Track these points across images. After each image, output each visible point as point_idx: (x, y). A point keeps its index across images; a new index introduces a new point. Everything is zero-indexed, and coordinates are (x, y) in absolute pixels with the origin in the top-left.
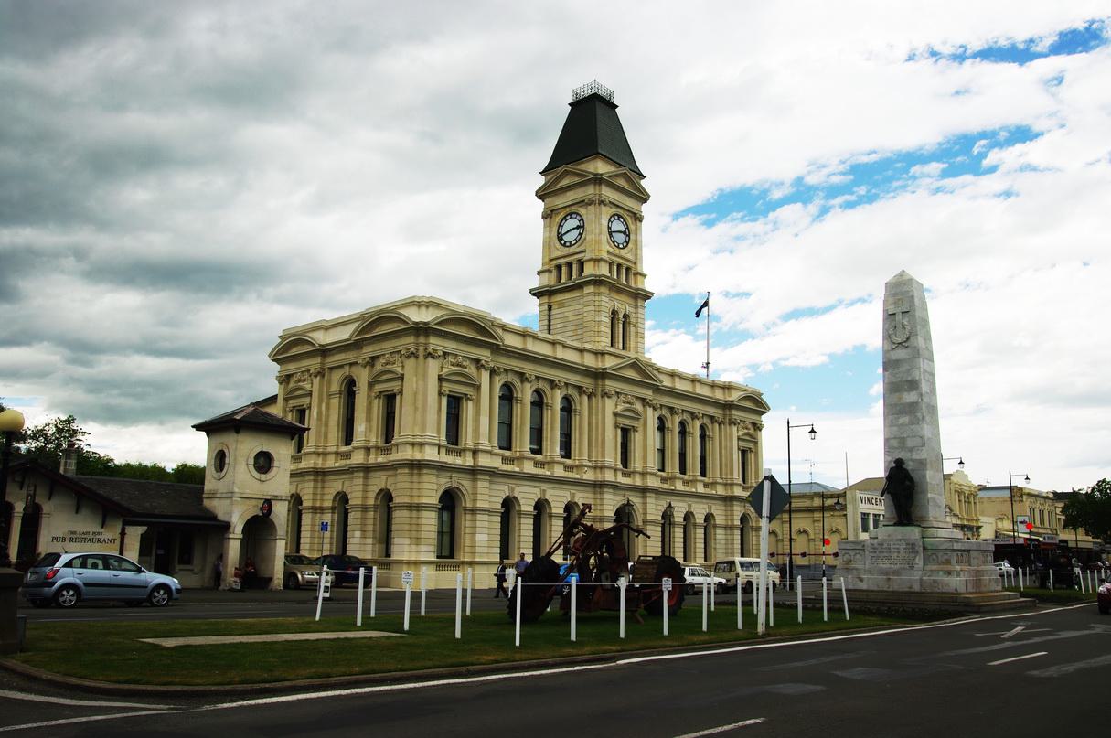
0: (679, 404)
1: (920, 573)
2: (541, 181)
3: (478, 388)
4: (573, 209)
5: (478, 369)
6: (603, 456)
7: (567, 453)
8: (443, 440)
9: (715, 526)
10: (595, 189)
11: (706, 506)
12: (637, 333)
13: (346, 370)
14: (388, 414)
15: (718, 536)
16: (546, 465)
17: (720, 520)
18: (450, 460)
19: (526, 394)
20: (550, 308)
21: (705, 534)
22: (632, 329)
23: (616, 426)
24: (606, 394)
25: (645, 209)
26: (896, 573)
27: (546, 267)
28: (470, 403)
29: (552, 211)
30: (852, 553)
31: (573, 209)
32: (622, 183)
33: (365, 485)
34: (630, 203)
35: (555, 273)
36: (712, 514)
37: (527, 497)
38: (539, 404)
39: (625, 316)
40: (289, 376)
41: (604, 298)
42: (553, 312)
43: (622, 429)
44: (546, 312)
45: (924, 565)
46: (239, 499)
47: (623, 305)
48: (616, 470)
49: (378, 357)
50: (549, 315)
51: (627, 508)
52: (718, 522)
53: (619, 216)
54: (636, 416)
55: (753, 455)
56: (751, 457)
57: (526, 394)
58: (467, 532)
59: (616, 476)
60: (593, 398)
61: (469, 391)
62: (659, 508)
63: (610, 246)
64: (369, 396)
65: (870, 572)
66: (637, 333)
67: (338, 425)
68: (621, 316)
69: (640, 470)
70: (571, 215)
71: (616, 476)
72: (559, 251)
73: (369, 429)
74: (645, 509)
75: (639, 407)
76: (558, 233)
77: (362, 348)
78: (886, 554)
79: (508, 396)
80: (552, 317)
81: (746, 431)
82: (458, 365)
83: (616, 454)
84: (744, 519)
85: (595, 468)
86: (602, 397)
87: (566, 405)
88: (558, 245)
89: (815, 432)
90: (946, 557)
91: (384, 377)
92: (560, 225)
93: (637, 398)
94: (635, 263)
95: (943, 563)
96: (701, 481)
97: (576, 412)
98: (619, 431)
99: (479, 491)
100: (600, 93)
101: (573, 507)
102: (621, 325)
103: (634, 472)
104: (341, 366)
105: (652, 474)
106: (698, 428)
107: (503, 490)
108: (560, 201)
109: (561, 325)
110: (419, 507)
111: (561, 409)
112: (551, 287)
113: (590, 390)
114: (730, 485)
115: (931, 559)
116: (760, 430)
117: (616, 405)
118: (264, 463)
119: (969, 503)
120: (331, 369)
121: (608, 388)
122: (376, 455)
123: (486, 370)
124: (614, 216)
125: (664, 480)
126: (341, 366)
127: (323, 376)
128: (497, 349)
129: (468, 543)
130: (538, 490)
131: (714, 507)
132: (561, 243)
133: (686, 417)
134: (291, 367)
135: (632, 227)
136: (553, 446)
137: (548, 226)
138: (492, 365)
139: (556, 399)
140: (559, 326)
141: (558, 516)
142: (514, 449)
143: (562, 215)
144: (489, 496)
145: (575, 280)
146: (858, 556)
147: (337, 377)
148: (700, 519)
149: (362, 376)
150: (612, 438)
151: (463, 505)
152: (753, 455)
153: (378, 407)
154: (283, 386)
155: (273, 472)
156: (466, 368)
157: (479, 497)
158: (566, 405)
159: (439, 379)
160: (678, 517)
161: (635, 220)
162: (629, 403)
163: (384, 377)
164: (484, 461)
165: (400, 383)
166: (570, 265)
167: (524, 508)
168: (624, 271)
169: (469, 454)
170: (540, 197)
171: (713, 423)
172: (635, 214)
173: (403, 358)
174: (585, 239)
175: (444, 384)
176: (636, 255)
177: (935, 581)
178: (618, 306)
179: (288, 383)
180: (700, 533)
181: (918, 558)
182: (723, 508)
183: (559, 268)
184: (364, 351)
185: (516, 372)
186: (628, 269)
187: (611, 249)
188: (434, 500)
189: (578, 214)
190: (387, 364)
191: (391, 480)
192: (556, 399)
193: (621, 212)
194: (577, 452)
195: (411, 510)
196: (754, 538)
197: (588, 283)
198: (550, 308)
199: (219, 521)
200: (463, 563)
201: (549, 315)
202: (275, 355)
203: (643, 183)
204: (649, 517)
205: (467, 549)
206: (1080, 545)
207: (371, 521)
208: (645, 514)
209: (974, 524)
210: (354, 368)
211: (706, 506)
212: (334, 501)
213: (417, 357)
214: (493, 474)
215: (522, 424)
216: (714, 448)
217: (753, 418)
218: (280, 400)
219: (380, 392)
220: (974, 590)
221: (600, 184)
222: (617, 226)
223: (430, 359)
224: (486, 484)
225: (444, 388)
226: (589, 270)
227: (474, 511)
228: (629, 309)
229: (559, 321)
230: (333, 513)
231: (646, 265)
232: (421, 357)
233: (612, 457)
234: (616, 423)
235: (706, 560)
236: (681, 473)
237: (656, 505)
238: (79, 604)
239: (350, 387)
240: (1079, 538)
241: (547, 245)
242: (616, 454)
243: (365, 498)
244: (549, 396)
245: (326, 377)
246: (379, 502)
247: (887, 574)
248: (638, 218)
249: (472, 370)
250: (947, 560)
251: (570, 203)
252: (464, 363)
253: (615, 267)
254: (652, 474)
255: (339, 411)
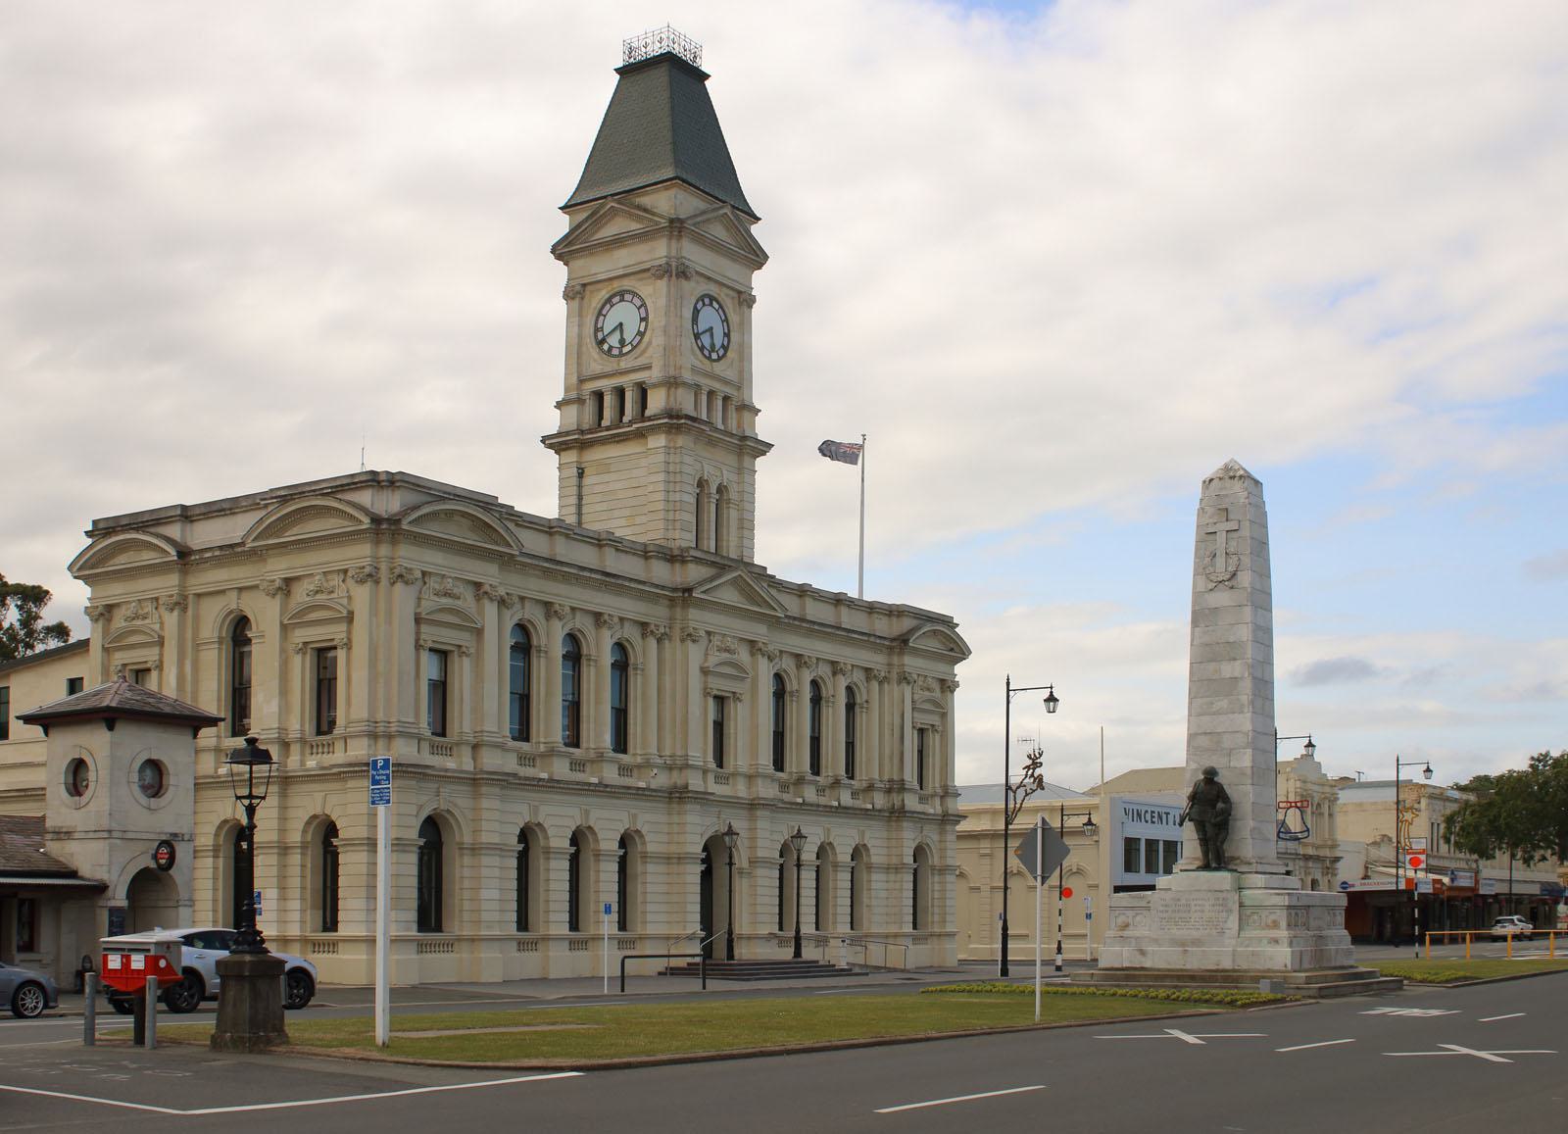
0: (566, 595)
1: (1234, 942)
2: (562, 225)
3: (479, 632)
4: (626, 284)
5: (478, 598)
6: (685, 747)
7: (621, 743)
8: (424, 727)
9: (869, 867)
10: (669, 246)
11: (576, 812)
12: (741, 520)
13: (231, 602)
14: (320, 682)
15: (874, 885)
16: (588, 765)
17: (877, 856)
18: (428, 759)
19: (552, 641)
20: (581, 475)
21: (817, 880)
22: (733, 514)
23: (706, 693)
24: (689, 635)
25: (761, 282)
26: (1197, 942)
27: (573, 395)
28: (466, 661)
29: (584, 285)
30: (1130, 913)
31: (626, 284)
32: (718, 232)
33: (283, 808)
34: (729, 270)
35: (590, 407)
36: (830, 844)
37: (558, 821)
38: (574, 657)
39: (720, 490)
40: (110, 608)
41: (688, 459)
42: (587, 481)
43: (716, 697)
44: (574, 481)
45: (1240, 929)
46: (118, 841)
47: (717, 467)
48: (705, 772)
49: (297, 578)
50: (580, 487)
51: (727, 839)
52: (875, 859)
53: (712, 299)
54: (740, 673)
55: (937, 737)
56: (934, 741)
57: (552, 641)
58: (936, 897)
59: (705, 782)
60: (886, 685)
61: (464, 638)
62: (776, 837)
63: (697, 359)
64: (283, 650)
65: (1156, 941)
66: (741, 520)
67: (219, 700)
68: (714, 490)
69: (744, 770)
70: (621, 294)
71: (705, 782)
72: (596, 363)
73: (284, 709)
74: (753, 839)
75: (743, 655)
76: (597, 330)
77: (265, 560)
78: (1184, 915)
79: (524, 647)
80: (585, 491)
81: (726, 655)
82: (447, 594)
83: (705, 743)
84: (919, 853)
85: (670, 768)
86: (683, 640)
87: (571, 649)
88: (594, 352)
89: (1056, 700)
90: (1272, 917)
91: (314, 616)
92: (600, 314)
93: (742, 639)
94: (739, 389)
95: (1268, 927)
96: (612, 761)
97: (539, 651)
98: (916, 732)
99: (485, 815)
100: (677, 50)
101: (584, 834)
102: (713, 508)
103: (734, 775)
104: (223, 592)
105: (765, 776)
106: (844, 688)
107: (519, 812)
108: (601, 266)
109: (604, 506)
110: (887, 869)
111: (564, 656)
112: (582, 432)
113: (662, 630)
114: (897, 787)
115: (1251, 921)
116: (952, 692)
117: (706, 655)
118: (154, 778)
119: (1321, 814)
120: (199, 596)
121: (692, 624)
122: (302, 754)
123: (491, 600)
124: (702, 298)
125: (525, 759)
126: (223, 592)
127: (185, 609)
128: (506, 561)
129: (467, 905)
130: (526, 807)
131: (868, 835)
132: (602, 350)
133: (824, 671)
134: (115, 591)
135: (733, 318)
136: (598, 729)
137: (576, 317)
138: (502, 591)
139: (601, 650)
140: (598, 507)
141: (559, 852)
142: (534, 739)
143: (604, 294)
144: (763, 838)
145: (631, 423)
146: (1138, 918)
147: (212, 619)
148: (844, 855)
149: (265, 616)
150: (700, 715)
151: (457, 839)
152: (937, 737)
153: (301, 671)
154: (100, 624)
155: (169, 795)
156: (459, 598)
157: (485, 825)
158: (571, 649)
159: (416, 619)
160: (809, 855)
161: (740, 304)
162: (728, 650)
163: (314, 616)
164: (491, 761)
165: (345, 629)
166: (620, 393)
167: (651, 848)
168: (720, 403)
169: (467, 752)
170: (559, 257)
171: (644, 636)
172: (740, 293)
173: (162, 609)
174: (650, 343)
175: (424, 628)
176: (741, 372)
177: (1253, 954)
178: (709, 471)
179: (109, 621)
180: (843, 879)
181: (1231, 918)
182: (885, 834)
183: (599, 396)
184: (269, 567)
185: (538, 601)
186: (726, 399)
187: (697, 363)
188: (697, 848)
189: (635, 294)
190: (317, 592)
191: (333, 799)
192: (601, 650)
193: (713, 289)
194: (639, 740)
195: (888, 873)
196: (937, 887)
197: (654, 429)
198: (581, 475)
199: (82, 878)
200: (460, 939)
201: (580, 487)
202: (79, 569)
203: (755, 229)
204: (760, 854)
205: (466, 916)
206: (1517, 889)
207: (297, 870)
208: (753, 848)
209: (1326, 853)
210: (245, 595)
211: (576, 812)
212: (217, 835)
213: (377, 582)
214: (506, 782)
215: (549, 694)
216: (869, 725)
217: (939, 669)
218: (96, 648)
219: (306, 644)
220: (1312, 967)
221: (680, 237)
222: (709, 317)
223: (399, 586)
224: (496, 804)
225: (423, 636)
226: (656, 402)
227: (475, 850)
228: (728, 477)
229: (598, 498)
230: (215, 857)
231: (557, 309)
232: (384, 582)
233: (700, 750)
234: (705, 689)
235: (915, 928)
236: (615, 750)
237: (772, 832)
238: (45, 1012)
239: (239, 632)
240: (1516, 876)
241: (575, 353)
242: (705, 743)
243: (282, 831)
244: (542, 632)
245: (190, 612)
246: (309, 838)
247: (1183, 944)
248: (746, 300)
249: (467, 602)
250: (1274, 922)
251: (621, 272)
252: (455, 591)
253: (704, 398)
254: (765, 776)
255: (219, 674)
